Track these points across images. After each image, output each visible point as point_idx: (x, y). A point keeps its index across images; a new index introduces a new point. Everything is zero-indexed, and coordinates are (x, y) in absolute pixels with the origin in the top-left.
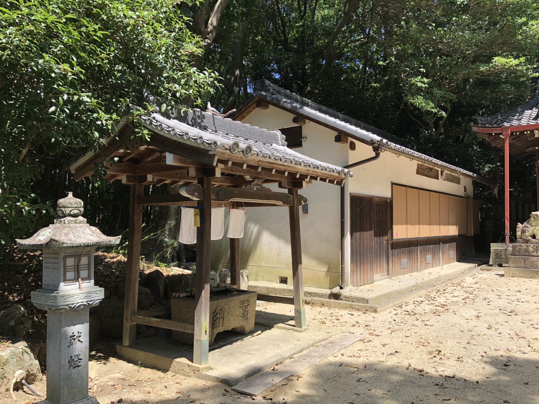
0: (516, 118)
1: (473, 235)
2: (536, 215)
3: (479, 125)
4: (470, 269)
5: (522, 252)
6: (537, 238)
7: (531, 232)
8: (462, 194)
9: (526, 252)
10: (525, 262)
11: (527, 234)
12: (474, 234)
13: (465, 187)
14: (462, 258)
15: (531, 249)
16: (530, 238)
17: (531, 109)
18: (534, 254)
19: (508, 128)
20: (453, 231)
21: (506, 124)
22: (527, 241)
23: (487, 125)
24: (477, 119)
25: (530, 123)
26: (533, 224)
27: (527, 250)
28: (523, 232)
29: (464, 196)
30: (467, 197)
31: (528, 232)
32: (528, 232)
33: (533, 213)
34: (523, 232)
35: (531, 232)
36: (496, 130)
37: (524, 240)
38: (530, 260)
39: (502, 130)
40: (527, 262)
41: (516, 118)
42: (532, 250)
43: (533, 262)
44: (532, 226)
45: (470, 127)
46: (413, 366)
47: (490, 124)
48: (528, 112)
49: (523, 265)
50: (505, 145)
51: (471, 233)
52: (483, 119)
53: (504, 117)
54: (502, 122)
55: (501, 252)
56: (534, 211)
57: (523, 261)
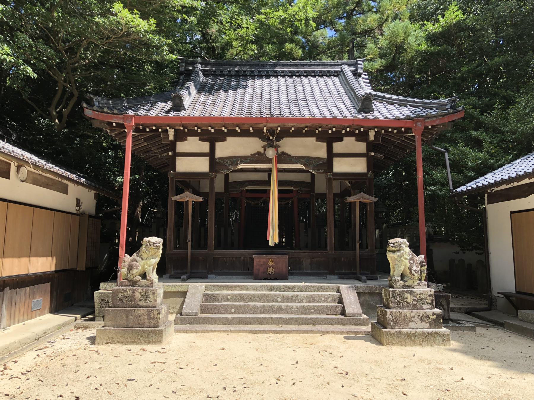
0: (145, 108)
1: (84, 270)
2: (149, 242)
3: (95, 108)
4: (60, 327)
5: (125, 300)
6: (148, 277)
7: (140, 268)
8: (73, 208)
9: (131, 301)
10: (127, 317)
11: (135, 271)
12: (86, 269)
13: (78, 201)
14: (57, 308)
15: (138, 296)
16: (139, 278)
17: (166, 102)
18: (142, 303)
19: (132, 116)
20: (44, 265)
21: (131, 112)
22: (134, 283)
23: (106, 110)
24: (92, 99)
25: (159, 115)
26: (145, 256)
27: (132, 298)
28: (130, 268)
29: (75, 212)
30: (81, 215)
31: (137, 268)
32: (137, 268)
33: (145, 239)
34: (130, 268)
35: (140, 268)
36: (116, 117)
37: (130, 281)
38: (135, 313)
39: (123, 118)
40: (130, 317)
41: (145, 108)
42: (140, 296)
43: (138, 316)
44: (142, 259)
45: (82, 108)
46: (160, 321)
47: (110, 109)
48: (161, 105)
49: (125, 322)
50: (127, 139)
51: (82, 266)
52: (101, 101)
53: (132, 105)
54: (127, 109)
55: (108, 297)
56: (148, 237)
57: (124, 316)
